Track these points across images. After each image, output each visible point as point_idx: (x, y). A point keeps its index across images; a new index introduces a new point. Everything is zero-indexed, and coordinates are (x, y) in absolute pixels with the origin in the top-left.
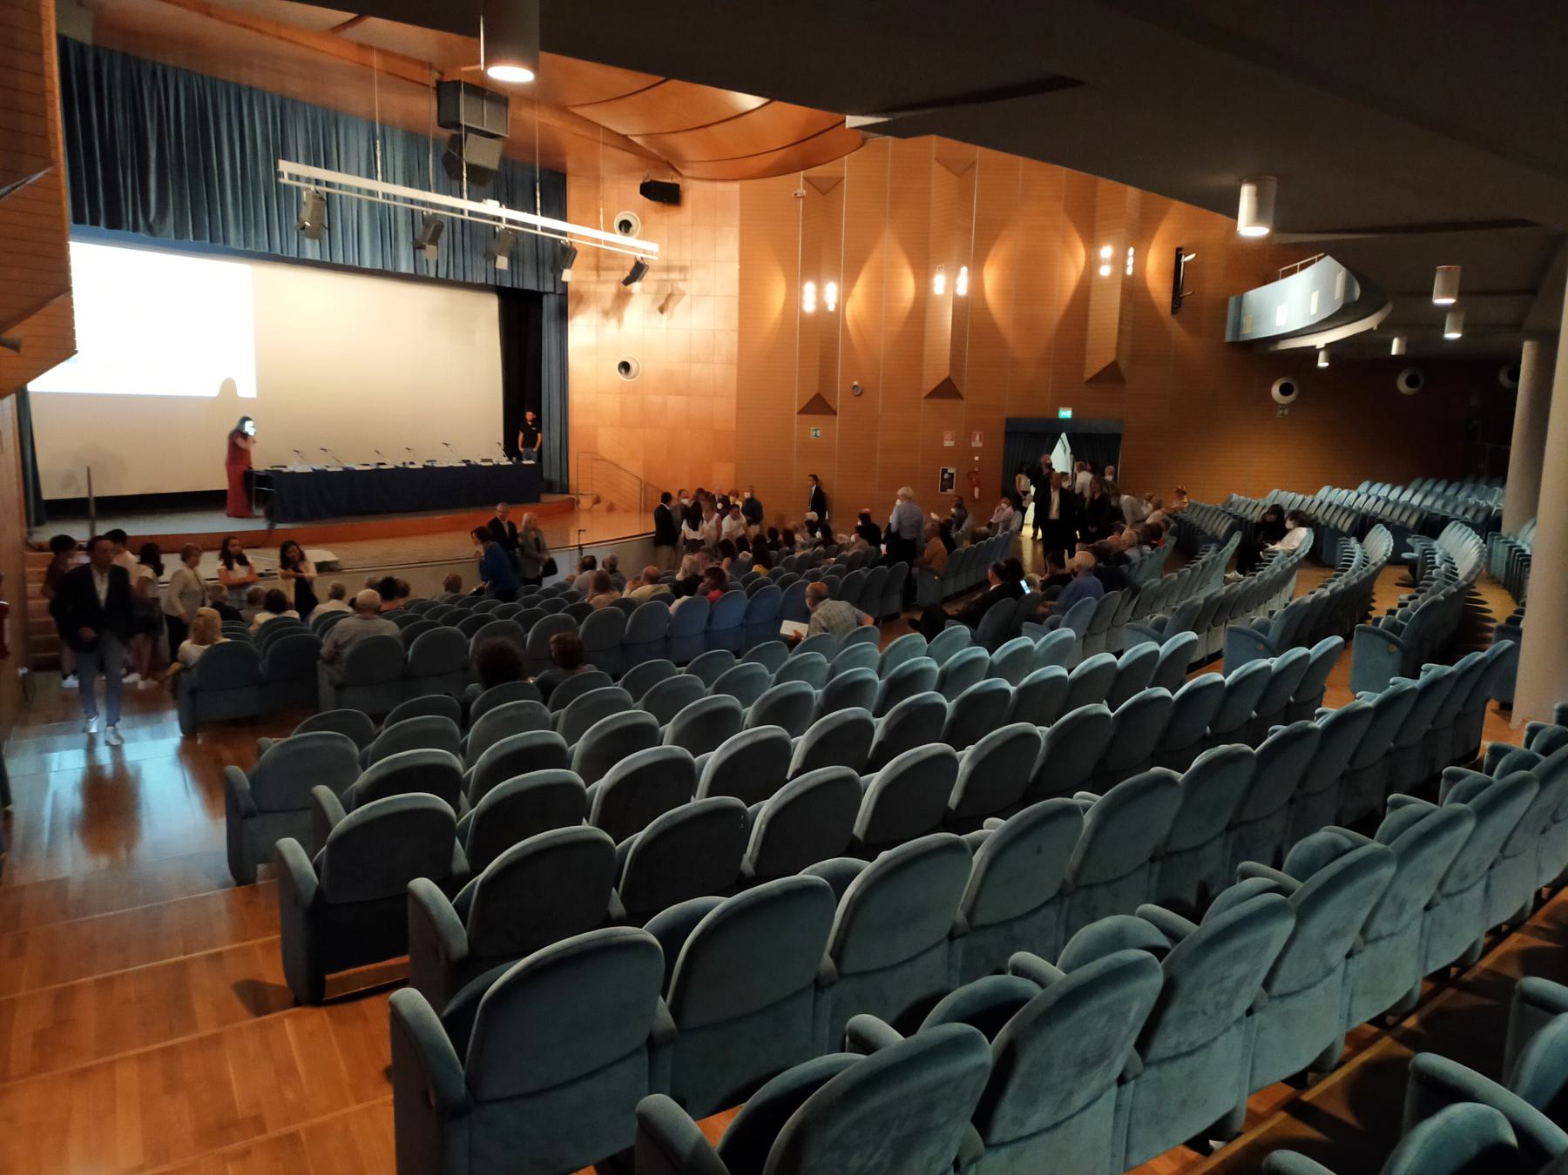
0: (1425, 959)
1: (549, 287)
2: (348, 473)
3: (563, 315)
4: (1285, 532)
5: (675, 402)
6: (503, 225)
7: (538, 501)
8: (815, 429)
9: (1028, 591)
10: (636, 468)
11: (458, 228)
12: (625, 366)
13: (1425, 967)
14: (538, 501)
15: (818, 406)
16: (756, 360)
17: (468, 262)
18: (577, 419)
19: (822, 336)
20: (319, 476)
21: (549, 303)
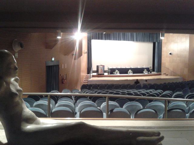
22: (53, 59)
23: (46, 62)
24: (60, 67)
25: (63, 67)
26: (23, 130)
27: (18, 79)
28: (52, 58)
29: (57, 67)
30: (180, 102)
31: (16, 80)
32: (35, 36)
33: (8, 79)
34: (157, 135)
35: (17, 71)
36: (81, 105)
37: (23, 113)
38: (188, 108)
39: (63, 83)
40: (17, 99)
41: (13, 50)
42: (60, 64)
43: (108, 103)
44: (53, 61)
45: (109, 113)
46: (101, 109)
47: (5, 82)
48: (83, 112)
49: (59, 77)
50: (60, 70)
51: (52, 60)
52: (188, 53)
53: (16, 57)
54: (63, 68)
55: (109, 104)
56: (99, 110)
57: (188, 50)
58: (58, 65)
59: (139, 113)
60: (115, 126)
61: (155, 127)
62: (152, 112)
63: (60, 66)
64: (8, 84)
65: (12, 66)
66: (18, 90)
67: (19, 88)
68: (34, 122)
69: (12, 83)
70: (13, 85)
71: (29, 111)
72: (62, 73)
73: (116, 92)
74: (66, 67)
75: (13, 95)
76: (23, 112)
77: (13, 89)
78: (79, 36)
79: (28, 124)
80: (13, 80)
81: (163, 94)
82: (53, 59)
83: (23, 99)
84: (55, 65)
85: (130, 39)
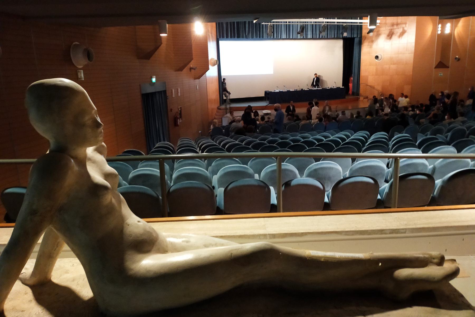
0: (68, 251)
1: (355, 36)
2: (289, 92)
3: (360, 43)
4: (457, 117)
5: (393, 67)
6: (324, 24)
7: (345, 98)
8: (441, 73)
9: (103, 143)
10: (379, 88)
11: (314, 27)
12: (377, 57)
13: (68, 251)
14: (345, 98)
15: (441, 65)
16: (420, 51)
17: (329, 33)
18: (363, 72)
19: (445, 43)
20: (280, 92)
21: (356, 40)
22: (154, 80)
23: (140, 85)
24: (167, 95)
25: (173, 93)
26: (131, 273)
27: (103, 146)
28: (152, 78)
29: (163, 93)
30: (438, 161)
31: (99, 150)
32: (113, 33)
33: (79, 152)
34: (436, 261)
35: (101, 129)
36: (223, 172)
37: (125, 229)
38: (432, 166)
39: (176, 124)
40: (109, 198)
41: (73, 64)
42: (167, 89)
43: (280, 166)
44: (154, 83)
45: (283, 188)
46: (261, 179)
47: (72, 158)
48: (231, 189)
49: (167, 114)
50: (168, 100)
51: (152, 81)
52: (413, 55)
53: (81, 78)
54: (174, 96)
55: (283, 167)
56: (262, 184)
57: (413, 49)
58: (165, 92)
59: (343, 186)
60: (320, 231)
61: (406, 229)
62: (368, 183)
63: (167, 92)
64: (82, 162)
65: (87, 118)
66: (107, 176)
67: (109, 169)
68: (155, 248)
69: (90, 159)
70: (94, 162)
71: (139, 222)
72: (174, 107)
73: (282, 139)
74: (179, 94)
75: (98, 189)
76: (125, 225)
77: (98, 178)
78: (199, 28)
79: (140, 256)
80: (90, 151)
81: (370, 141)
82: (154, 80)
83: (122, 194)
84: (159, 92)
85: (234, 34)
